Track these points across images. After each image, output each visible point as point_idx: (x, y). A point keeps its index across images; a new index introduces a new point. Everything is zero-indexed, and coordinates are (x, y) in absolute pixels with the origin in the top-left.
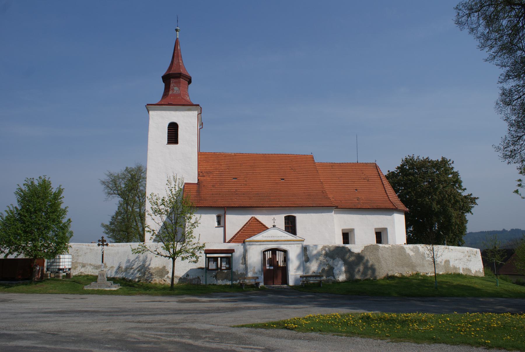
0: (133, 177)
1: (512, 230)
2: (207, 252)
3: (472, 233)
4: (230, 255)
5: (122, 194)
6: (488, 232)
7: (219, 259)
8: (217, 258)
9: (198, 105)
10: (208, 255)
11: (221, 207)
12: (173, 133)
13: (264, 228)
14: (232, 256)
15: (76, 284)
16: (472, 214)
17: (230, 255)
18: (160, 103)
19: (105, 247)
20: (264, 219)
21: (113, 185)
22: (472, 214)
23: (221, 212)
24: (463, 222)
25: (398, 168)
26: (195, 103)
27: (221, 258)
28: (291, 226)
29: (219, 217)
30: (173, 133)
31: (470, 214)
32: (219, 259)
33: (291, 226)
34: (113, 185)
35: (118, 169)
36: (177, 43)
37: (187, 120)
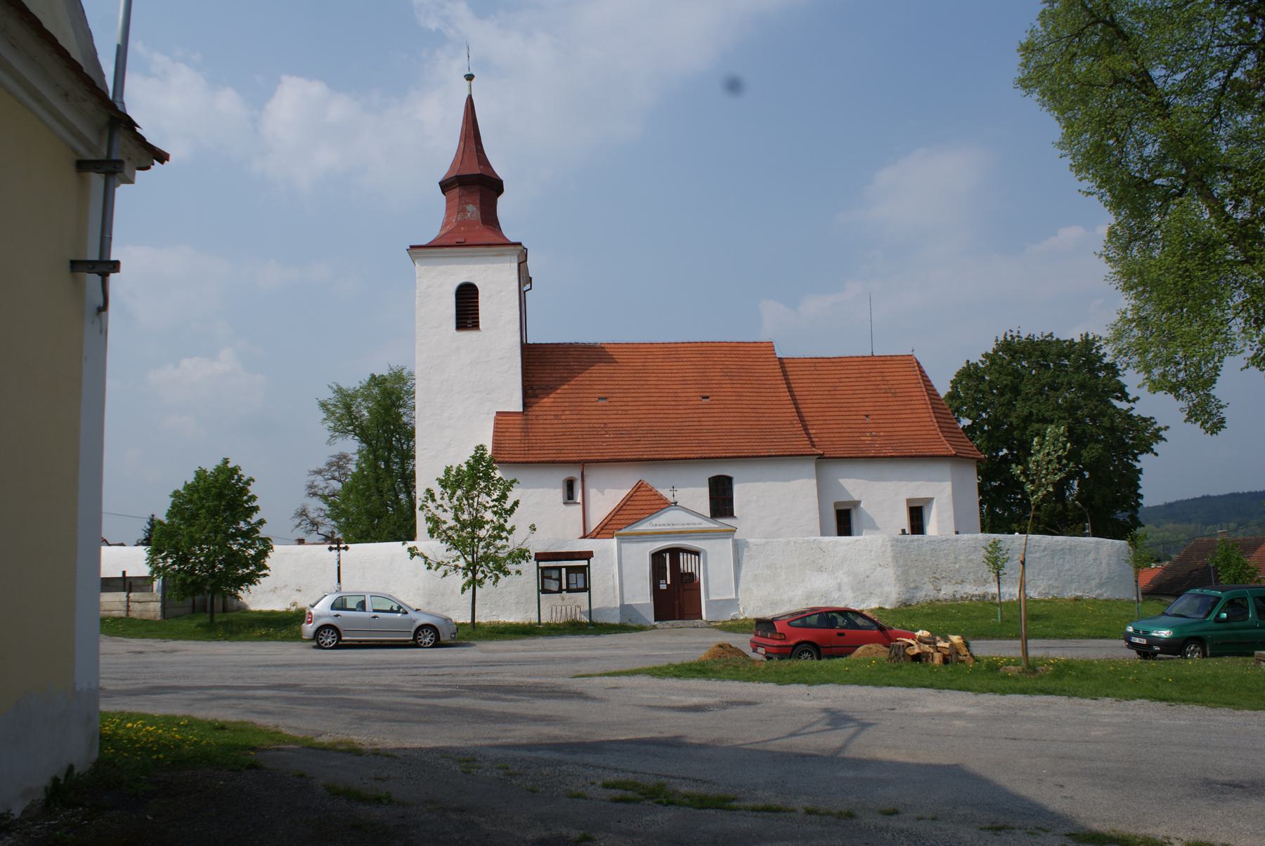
0: (387, 394)
1: (1203, 497)
2: (540, 557)
3: (1208, 497)
4: (584, 563)
5: (363, 434)
6: (1250, 493)
7: (564, 570)
8: (559, 568)
9: (520, 244)
10: (542, 564)
11: (575, 462)
12: (467, 307)
13: (663, 505)
14: (588, 566)
15: (284, 625)
16: (1156, 454)
17: (584, 563)
18: (442, 242)
19: (343, 552)
20: (661, 482)
21: (343, 413)
22: (1156, 454)
23: (575, 473)
24: (1132, 477)
25: (986, 356)
26: (513, 240)
27: (567, 568)
28: (721, 501)
29: (570, 485)
30: (467, 307)
31: (1150, 455)
32: (564, 570)
33: (721, 501)
34: (343, 413)
35: (354, 380)
36: (470, 101)
37: (494, 278)
